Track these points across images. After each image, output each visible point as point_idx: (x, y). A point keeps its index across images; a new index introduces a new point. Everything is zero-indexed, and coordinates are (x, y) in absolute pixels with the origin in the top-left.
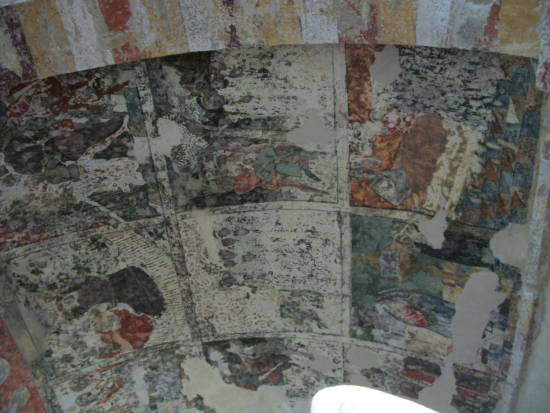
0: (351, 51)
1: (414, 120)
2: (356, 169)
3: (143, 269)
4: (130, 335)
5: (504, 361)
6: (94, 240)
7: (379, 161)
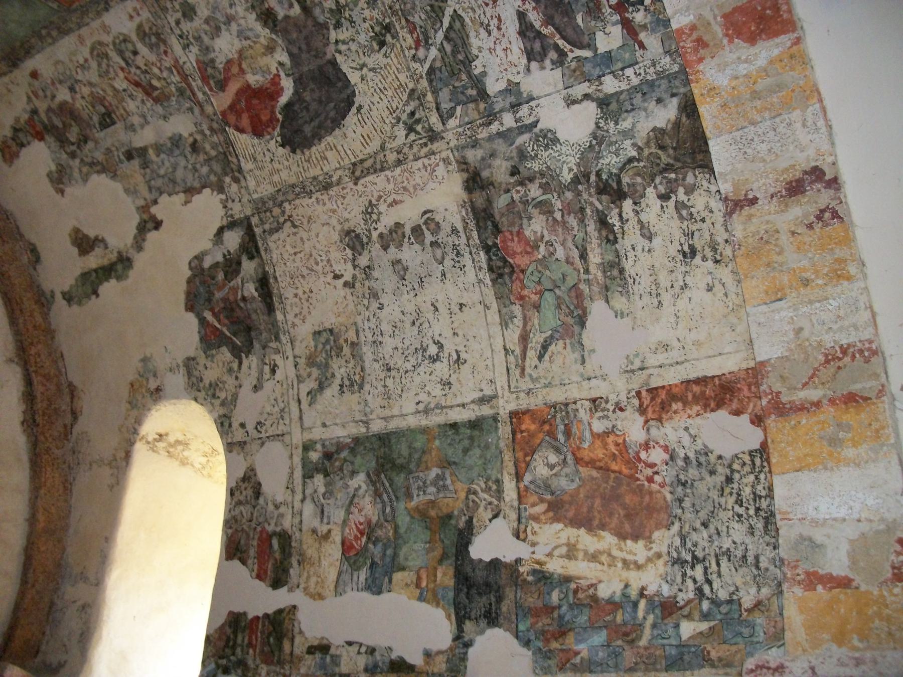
0: (744, 379)
1: (658, 487)
2: (567, 413)
3: (354, 110)
4: (243, 104)
6: (388, 28)
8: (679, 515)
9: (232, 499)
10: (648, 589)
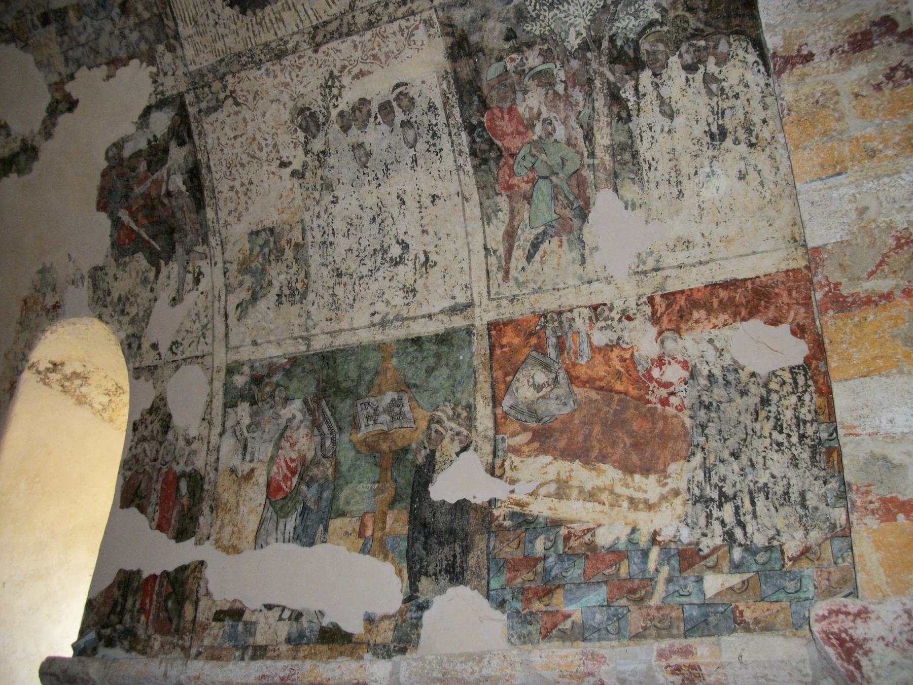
0: (783, 282)
1: (674, 411)
2: (561, 323)
5: (224, 652)
7: (583, 361)
8: (702, 444)
9: (134, 435)
10: (662, 534)
